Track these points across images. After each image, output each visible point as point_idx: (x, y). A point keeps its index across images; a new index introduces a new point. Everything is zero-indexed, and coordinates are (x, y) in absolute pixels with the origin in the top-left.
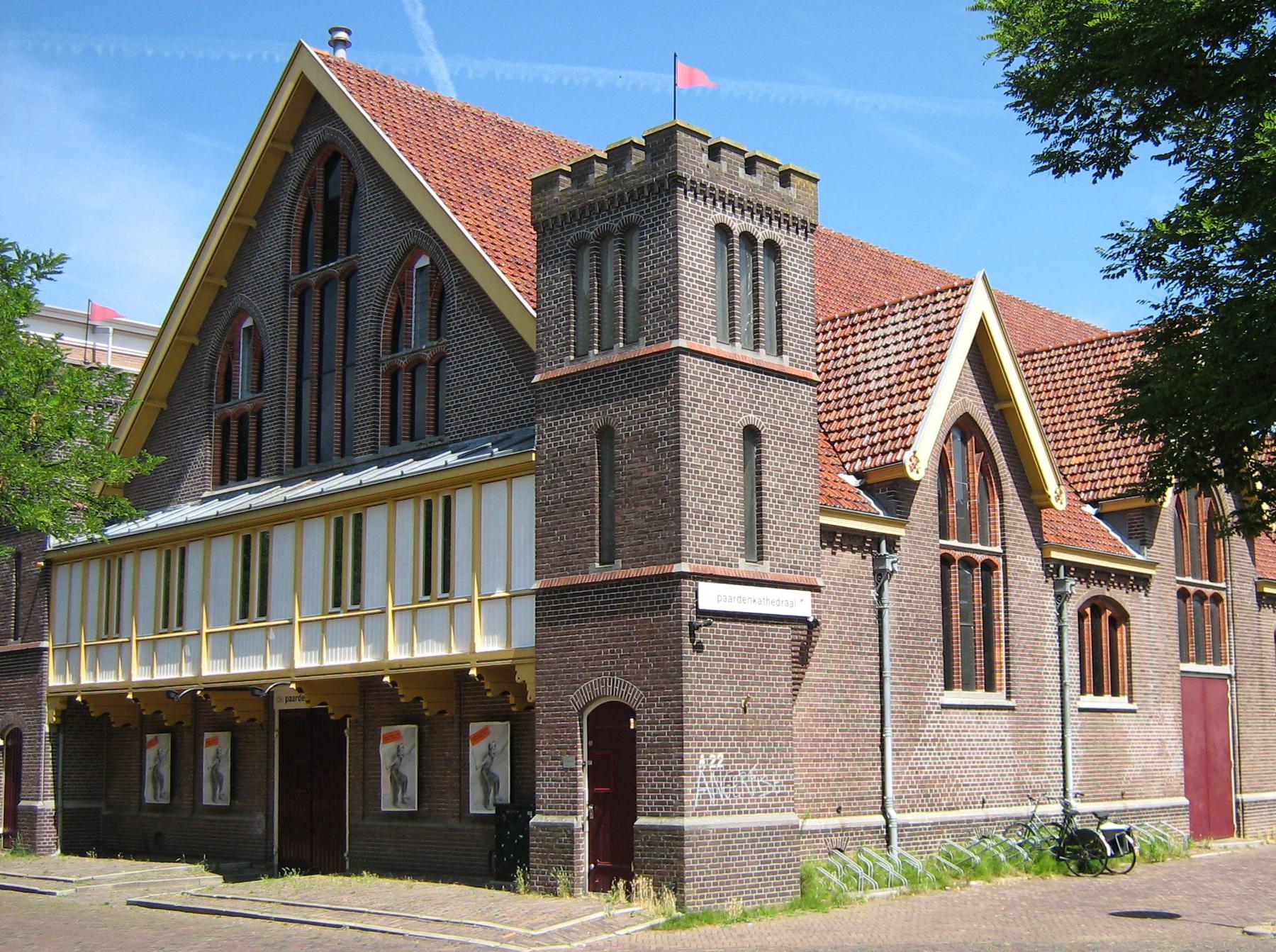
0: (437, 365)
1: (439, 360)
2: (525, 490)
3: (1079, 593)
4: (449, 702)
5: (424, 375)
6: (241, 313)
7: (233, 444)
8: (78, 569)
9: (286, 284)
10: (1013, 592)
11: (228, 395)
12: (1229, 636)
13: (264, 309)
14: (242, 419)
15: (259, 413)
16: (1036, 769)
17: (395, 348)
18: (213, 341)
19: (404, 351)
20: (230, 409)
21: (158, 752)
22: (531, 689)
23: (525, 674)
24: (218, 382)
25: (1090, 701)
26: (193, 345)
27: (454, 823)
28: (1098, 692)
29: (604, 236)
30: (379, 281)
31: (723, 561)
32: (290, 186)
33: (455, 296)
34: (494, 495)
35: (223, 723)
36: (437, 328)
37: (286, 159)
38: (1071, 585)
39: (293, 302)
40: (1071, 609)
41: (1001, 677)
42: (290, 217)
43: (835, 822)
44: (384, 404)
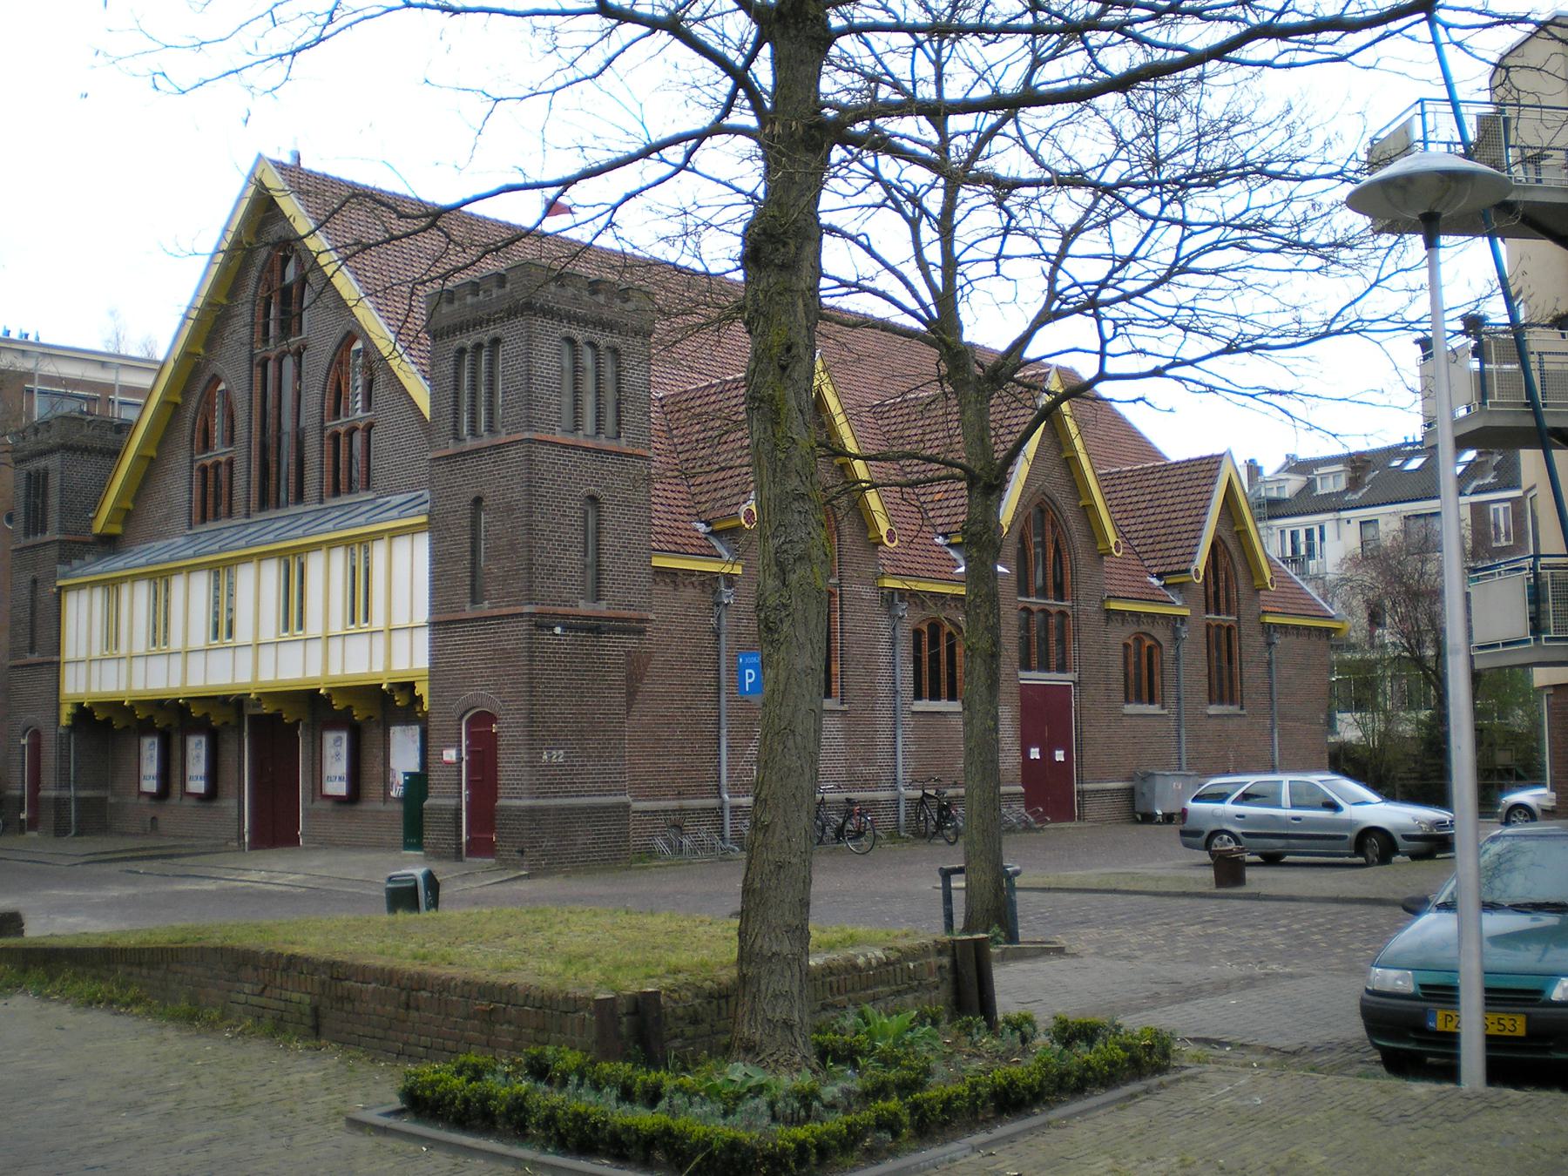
0: (369, 432)
1: (369, 427)
2: (423, 543)
3: (910, 617)
4: (372, 710)
5: (358, 438)
6: (216, 380)
7: (211, 489)
8: (84, 594)
9: (252, 356)
10: (848, 616)
11: (207, 446)
12: (1072, 648)
13: (234, 377)
14: (217, 465)
15: (230, 463)
16: (868, 761)
17: (337, 414)
18: (194, 403)
19: (343, 420)
20: (207, 459)
21: (150, 751)
22: (426, 700)
23: (422, 689)
24: (198, 436)
25: (924, 705)
26: (176, 404)
27: (381, 806)
28: (935, 696)
29: (478, 347)
30: (324, 360)
31: (565, 602)
32: (254, 273)
33: (381, 379)
34: (402, 545)
35: (202, 726)
36: (368, 405)
37: (250, 252)
38: (902, 609)
39: (258, 372)
40: (905, 632)
41: (836, 687)
42: (192, 440)
43: (674, 804)
44: (328, 462)
